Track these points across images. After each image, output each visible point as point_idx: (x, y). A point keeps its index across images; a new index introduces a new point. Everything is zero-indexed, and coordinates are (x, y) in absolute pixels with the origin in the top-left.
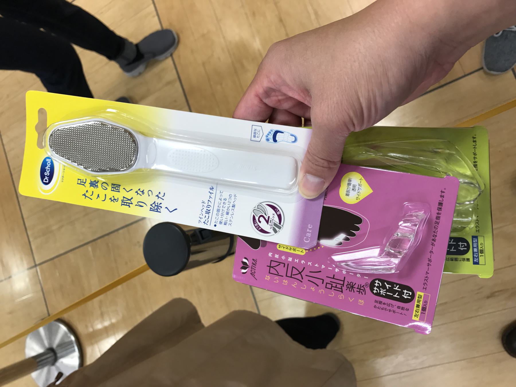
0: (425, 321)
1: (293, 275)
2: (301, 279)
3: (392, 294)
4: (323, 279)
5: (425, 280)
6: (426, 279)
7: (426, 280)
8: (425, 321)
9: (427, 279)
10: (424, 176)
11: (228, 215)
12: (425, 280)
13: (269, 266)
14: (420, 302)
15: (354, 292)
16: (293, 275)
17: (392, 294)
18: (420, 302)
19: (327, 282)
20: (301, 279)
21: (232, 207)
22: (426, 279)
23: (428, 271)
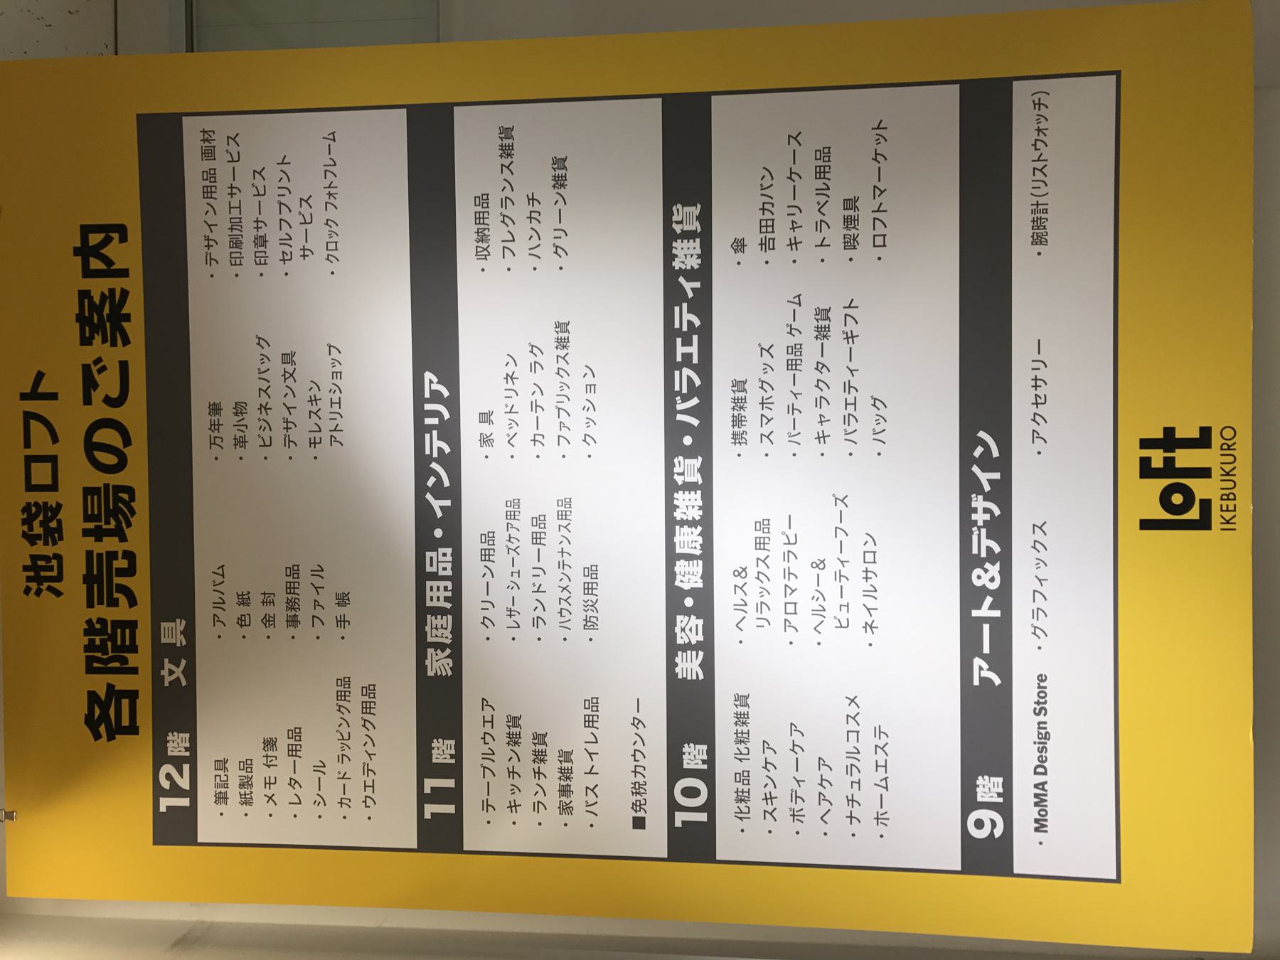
0: (111, 487)
1: (797, 811)
2: (1223, 466)
3: (986, 650)
4: (246, 402)
5: (1036, 171)
6: (1039, 165)
7: (1041, 170)
8: (111, 487)
9: (1043, 164)
10: (108, 916)
11: (251, 804)
12: (1036, 171)
13: (518, 806)
14: (370, 708)
15: (325, 805)
16: (797, 811)
17: (986, 650)
18: (370, 708)
19: (299, 805)
20: (1223, 466)
21: (241, 786)
22: (1039, 165)
23: (878, 185)
